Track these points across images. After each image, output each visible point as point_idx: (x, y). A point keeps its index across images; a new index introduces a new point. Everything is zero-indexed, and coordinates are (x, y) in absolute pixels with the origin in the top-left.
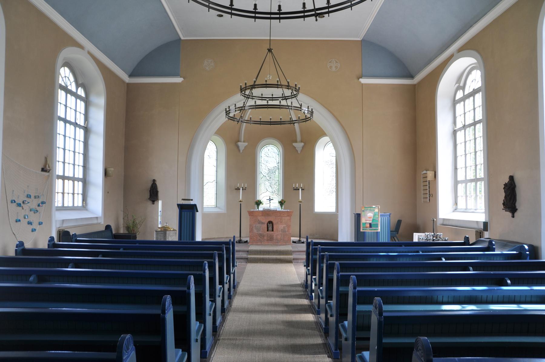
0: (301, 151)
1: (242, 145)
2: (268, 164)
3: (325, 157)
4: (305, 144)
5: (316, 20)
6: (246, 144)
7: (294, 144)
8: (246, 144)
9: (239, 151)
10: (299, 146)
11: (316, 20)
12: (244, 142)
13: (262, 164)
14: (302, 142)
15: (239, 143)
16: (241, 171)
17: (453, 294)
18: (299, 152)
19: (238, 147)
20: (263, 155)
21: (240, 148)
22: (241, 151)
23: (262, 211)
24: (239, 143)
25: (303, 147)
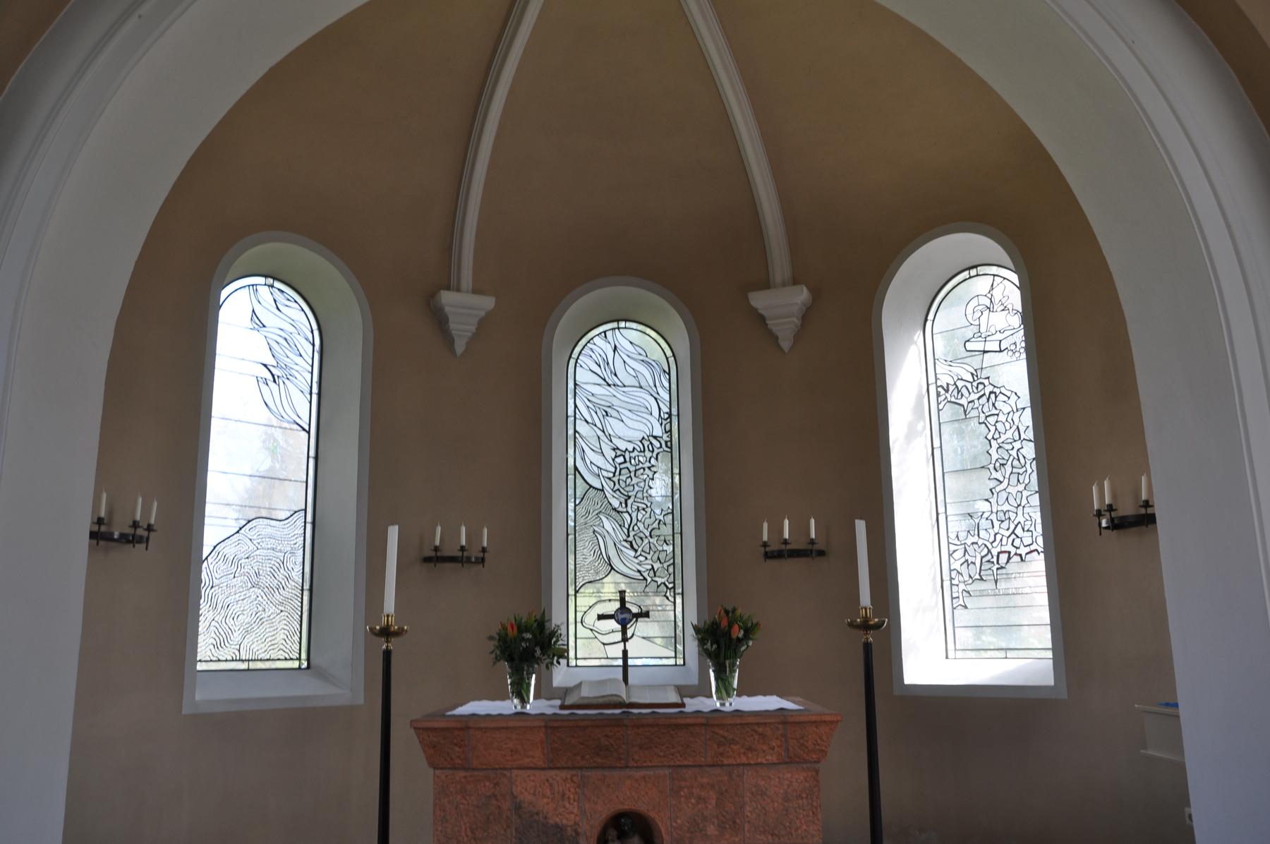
0: (798, 337)
1: (465, 307)
2: (613, 426)
3: (956, 358)
4: (815, 292)
5: (491, 638)
6: (488, 303)
7: (759, 300)
8: (488, 303)
9: (449, 340)
10: (783, 304)
11: (491, 638)
12: (476, 291)
13: (581, 427)
14: (795, 281)
15: (447, 297)
16: (444, 462)
17: (563, 631)
18: (786, 345)
19: (440, 320)
20: (583, 376)
21: (453, 326)
22: (460, 347)
23: (548, 723)
24: (447, 297)
25: (807, 315)
